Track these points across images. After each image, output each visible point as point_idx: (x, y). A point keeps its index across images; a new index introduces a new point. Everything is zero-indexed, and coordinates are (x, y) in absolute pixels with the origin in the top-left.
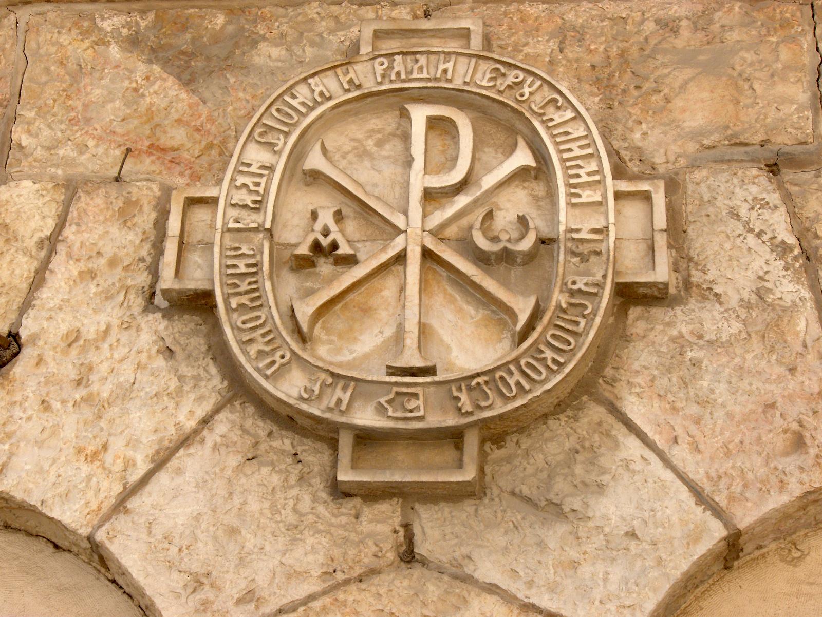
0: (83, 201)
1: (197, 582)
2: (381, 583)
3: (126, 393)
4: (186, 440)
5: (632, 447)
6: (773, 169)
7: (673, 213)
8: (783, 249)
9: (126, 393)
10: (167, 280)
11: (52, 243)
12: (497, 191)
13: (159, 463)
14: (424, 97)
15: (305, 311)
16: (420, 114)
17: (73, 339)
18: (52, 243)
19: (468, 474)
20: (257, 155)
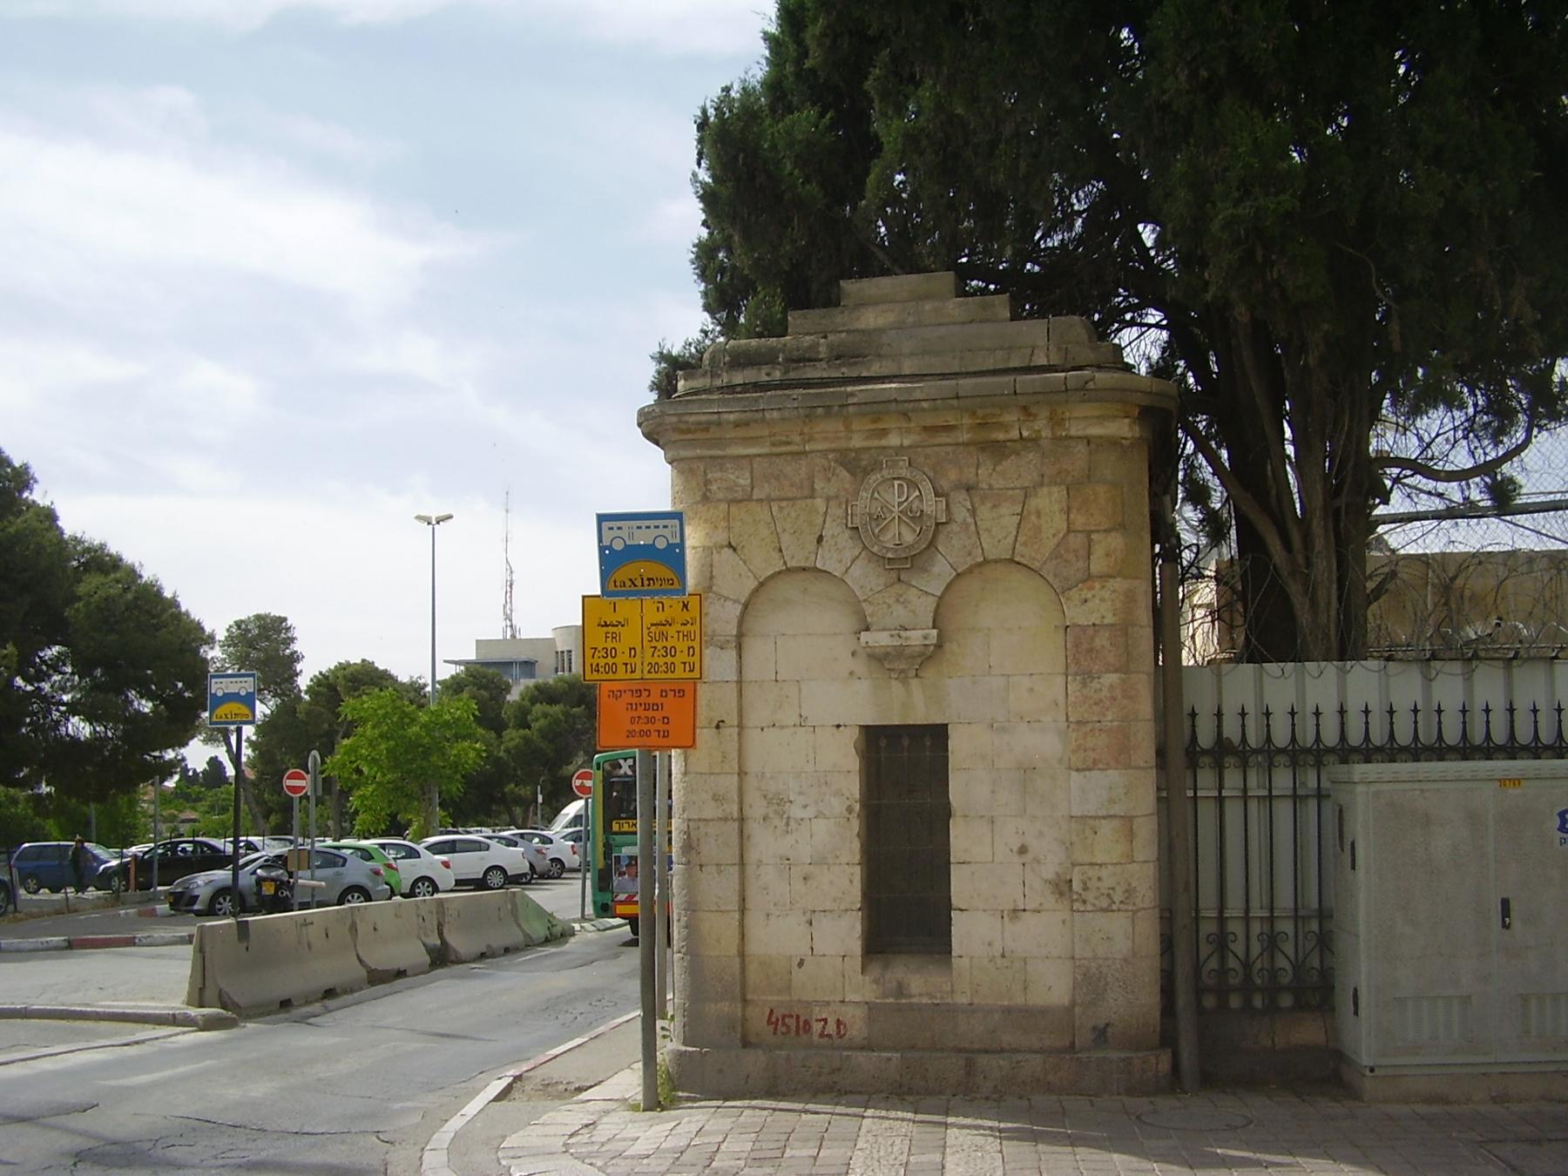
0: (831, 503)
1: (862, 587)
2: (895, 586)
3: (844, 548)
4: (857, 557)
5: (939, 555)
6: (968, 490)
7: (947, 505)
8: (968, 510)
9: (844, 548)
10: (849, 525)
11: (826, 512)
12: (31, 1115)
13: (853, 562)
14: (898, 479)
15: (877, 531)
16: (896, 483)
17: (833, 535)
18: (826, 512)
19: (908, 566)
20: (865, 494)
